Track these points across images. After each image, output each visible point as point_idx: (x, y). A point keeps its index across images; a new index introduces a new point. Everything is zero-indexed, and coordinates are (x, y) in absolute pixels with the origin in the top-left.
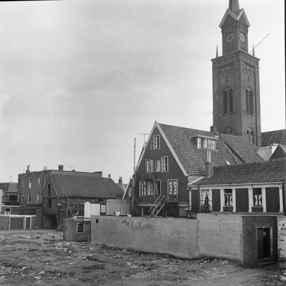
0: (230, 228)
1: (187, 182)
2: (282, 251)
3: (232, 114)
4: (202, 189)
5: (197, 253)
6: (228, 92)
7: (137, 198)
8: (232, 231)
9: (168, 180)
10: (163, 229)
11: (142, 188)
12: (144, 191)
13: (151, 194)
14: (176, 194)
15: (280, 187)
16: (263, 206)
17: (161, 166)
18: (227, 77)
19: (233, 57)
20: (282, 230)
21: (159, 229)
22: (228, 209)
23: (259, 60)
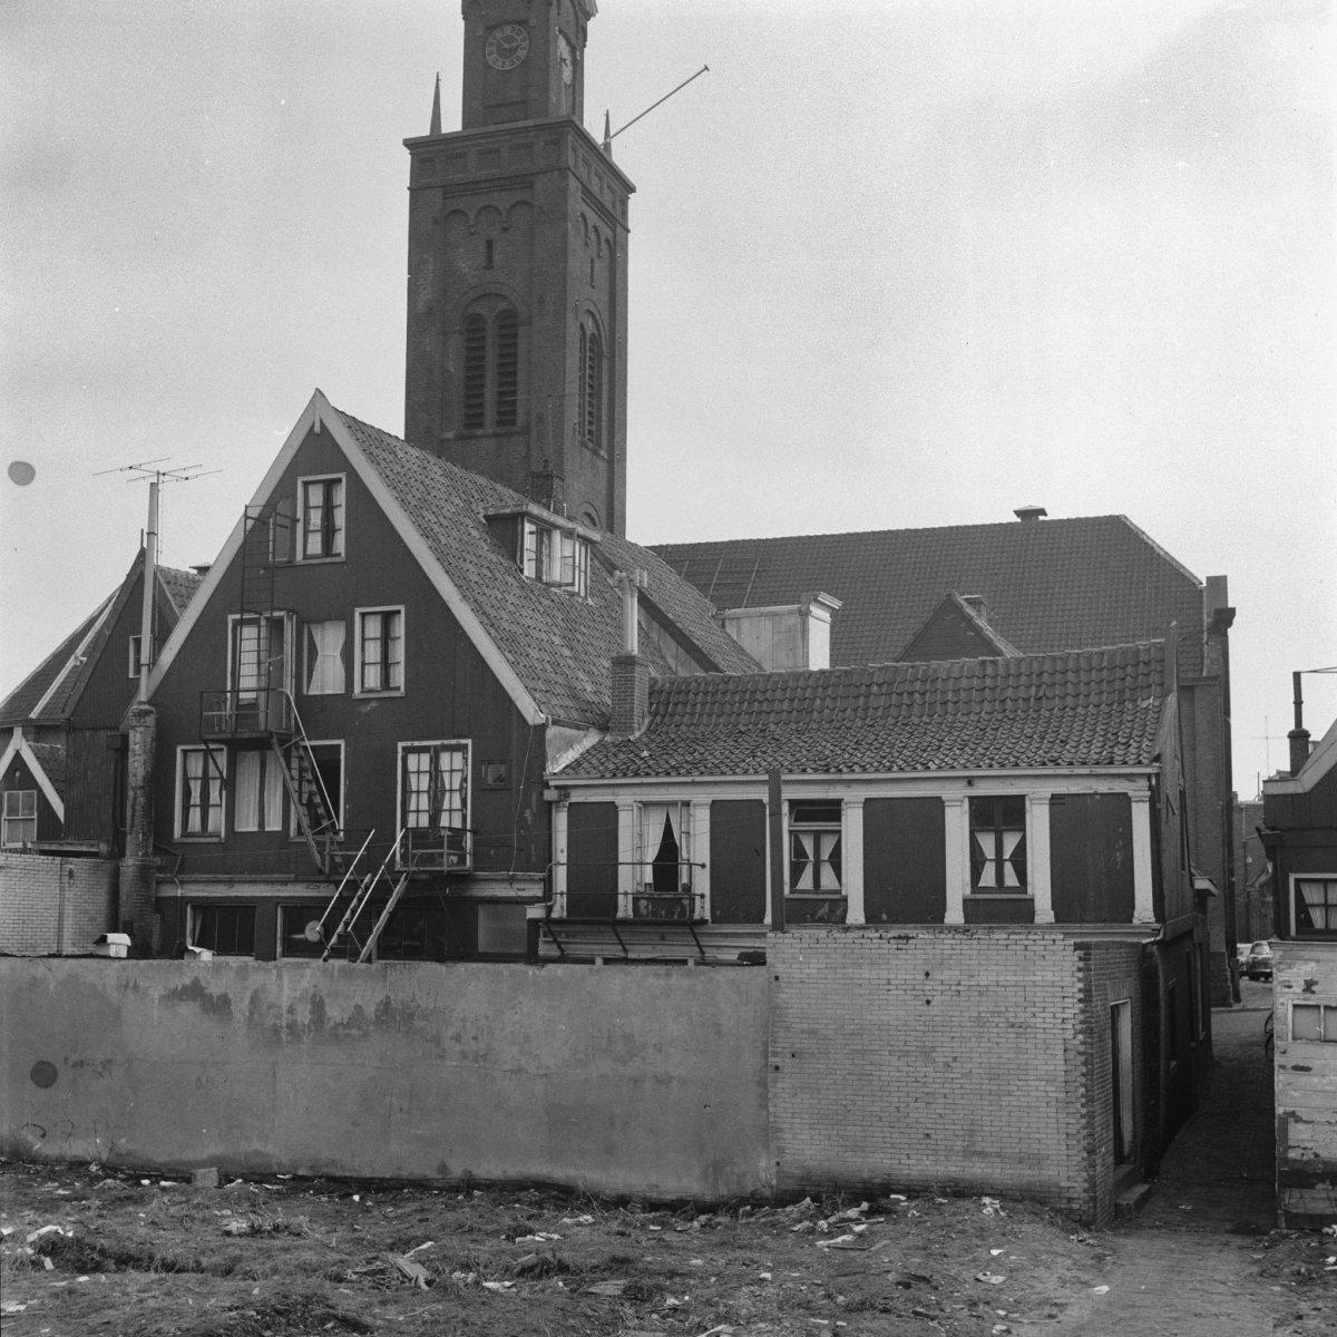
0: (998, 1009)
1: (541, 759)
2: (1300, 1126)
3: (512, 434)
4: (645, 799)
5: (763, 1163)
6: (494, 323)
7: (157, 850)
8: (1013, 1026)
9: (400, 745)
10: (508, 1030)
11: (196, 788)
12: (205, 805)
13: (262, 824)
14: (457, 824)
15: (1141, 793)
16: (843, 893)
17: (348, 661)
18: (490, 244)
19: (530, 146)
20: (1303, 1013)
21: (473, 1033)
22: (1000, 910)
23: (632, 190)
